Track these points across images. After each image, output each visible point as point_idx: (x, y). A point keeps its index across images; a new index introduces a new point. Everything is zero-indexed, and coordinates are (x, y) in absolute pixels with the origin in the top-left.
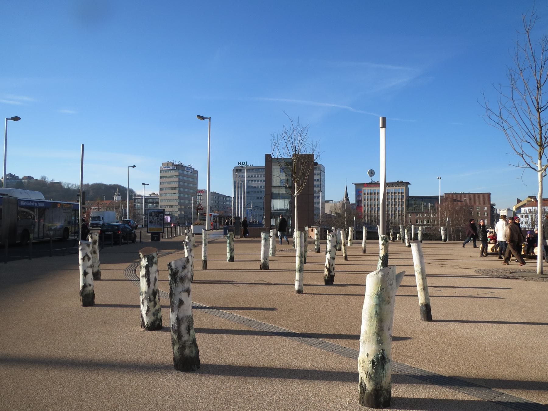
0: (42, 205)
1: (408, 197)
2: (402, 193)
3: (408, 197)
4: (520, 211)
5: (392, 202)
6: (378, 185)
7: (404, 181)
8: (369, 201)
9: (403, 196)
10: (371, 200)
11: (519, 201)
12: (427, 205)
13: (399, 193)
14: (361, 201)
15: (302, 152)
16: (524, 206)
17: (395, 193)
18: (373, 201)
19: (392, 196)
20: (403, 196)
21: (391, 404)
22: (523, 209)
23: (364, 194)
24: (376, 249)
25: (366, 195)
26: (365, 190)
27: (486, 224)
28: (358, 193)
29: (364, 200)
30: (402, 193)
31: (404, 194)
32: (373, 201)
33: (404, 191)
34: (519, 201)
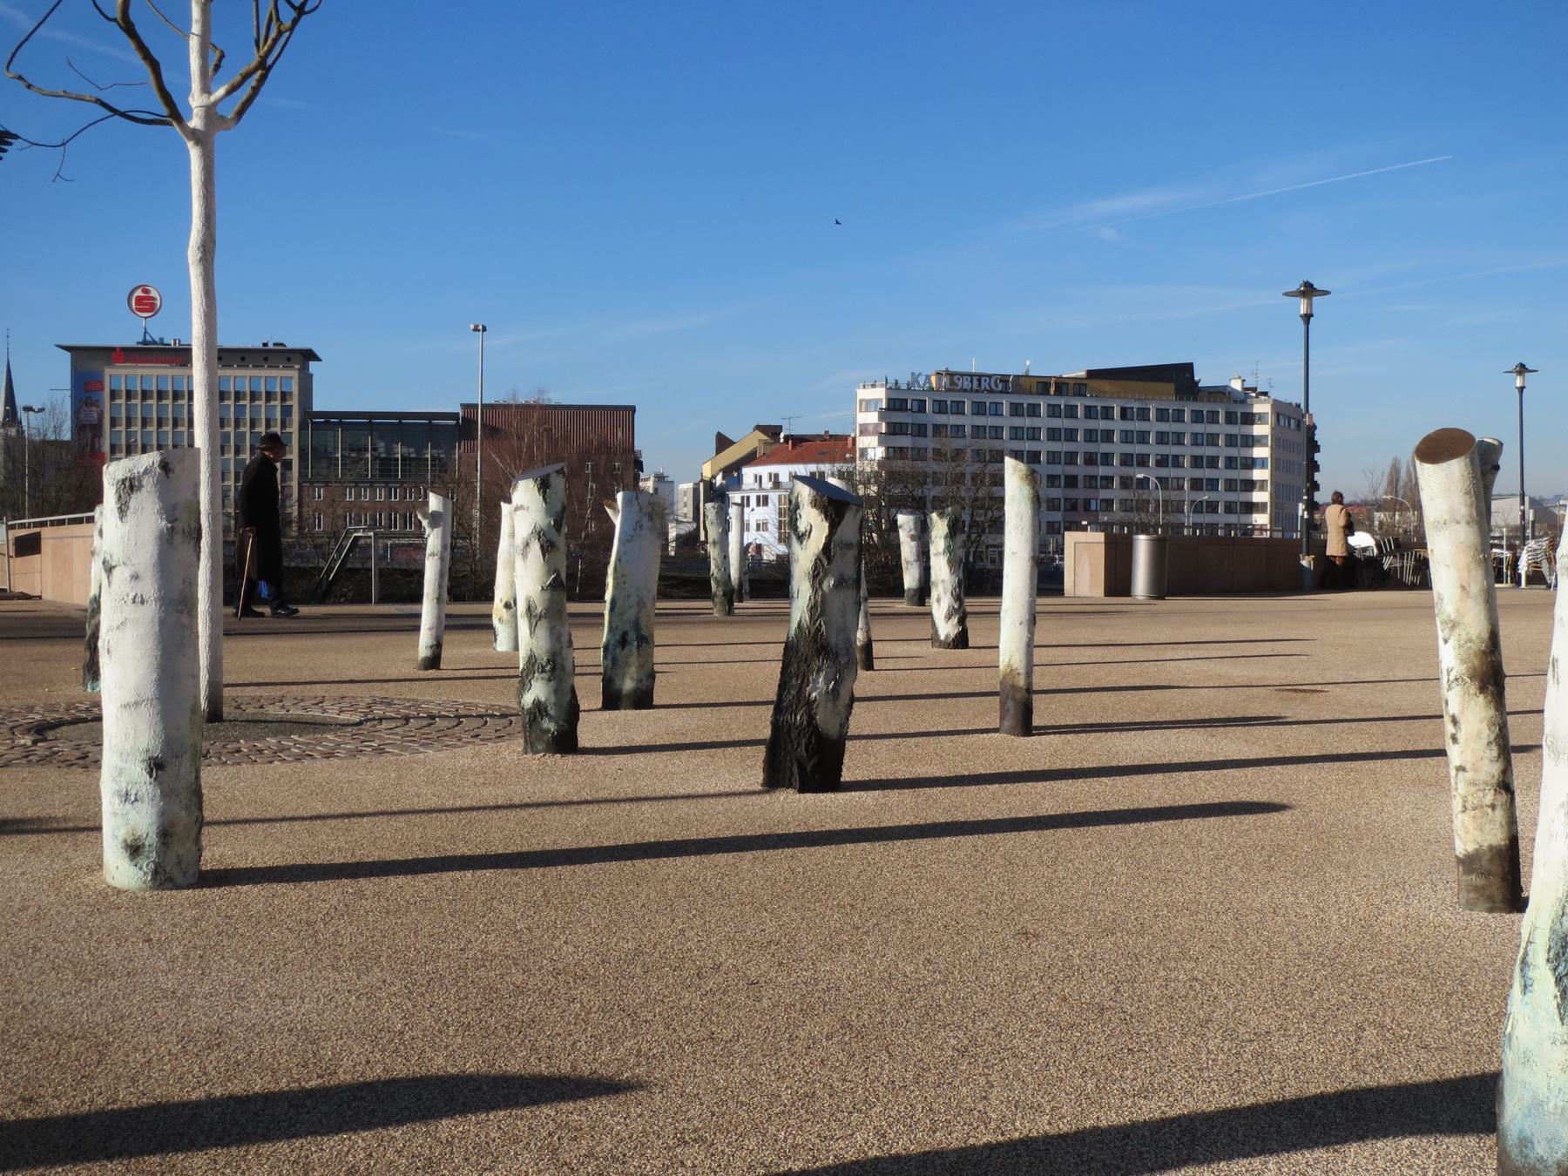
0: (702, 538)
1: (308, 415)
2: (285, 396)
3: (308, 415)
4: (739, 480)
5: (240, 437)
6: (181, 356)
7: (290, 345)
8: (137, 428)
9: (287, 411)
10: (145, 422)
11: (723, 443)
12: (389, 450)
13: (269, 396)
14: (97, 429)
15: (1471, 1141)
16: (750, 459)
17: (254, 396)
18: (168, 428)
19: (240, 410)
20: (287, 411)
21: (401, 561)
22: (748, 473)
23: (114, 395)
24: (70, 692)
25: (122, 401)
26: (116, 376)
27: (710, 540)
28: (85, 387)
29: (114, 422)
30: (285, 396)
31: (294, 402)
32: (153, 428)
33: (295, 389)
34: (723, 443)
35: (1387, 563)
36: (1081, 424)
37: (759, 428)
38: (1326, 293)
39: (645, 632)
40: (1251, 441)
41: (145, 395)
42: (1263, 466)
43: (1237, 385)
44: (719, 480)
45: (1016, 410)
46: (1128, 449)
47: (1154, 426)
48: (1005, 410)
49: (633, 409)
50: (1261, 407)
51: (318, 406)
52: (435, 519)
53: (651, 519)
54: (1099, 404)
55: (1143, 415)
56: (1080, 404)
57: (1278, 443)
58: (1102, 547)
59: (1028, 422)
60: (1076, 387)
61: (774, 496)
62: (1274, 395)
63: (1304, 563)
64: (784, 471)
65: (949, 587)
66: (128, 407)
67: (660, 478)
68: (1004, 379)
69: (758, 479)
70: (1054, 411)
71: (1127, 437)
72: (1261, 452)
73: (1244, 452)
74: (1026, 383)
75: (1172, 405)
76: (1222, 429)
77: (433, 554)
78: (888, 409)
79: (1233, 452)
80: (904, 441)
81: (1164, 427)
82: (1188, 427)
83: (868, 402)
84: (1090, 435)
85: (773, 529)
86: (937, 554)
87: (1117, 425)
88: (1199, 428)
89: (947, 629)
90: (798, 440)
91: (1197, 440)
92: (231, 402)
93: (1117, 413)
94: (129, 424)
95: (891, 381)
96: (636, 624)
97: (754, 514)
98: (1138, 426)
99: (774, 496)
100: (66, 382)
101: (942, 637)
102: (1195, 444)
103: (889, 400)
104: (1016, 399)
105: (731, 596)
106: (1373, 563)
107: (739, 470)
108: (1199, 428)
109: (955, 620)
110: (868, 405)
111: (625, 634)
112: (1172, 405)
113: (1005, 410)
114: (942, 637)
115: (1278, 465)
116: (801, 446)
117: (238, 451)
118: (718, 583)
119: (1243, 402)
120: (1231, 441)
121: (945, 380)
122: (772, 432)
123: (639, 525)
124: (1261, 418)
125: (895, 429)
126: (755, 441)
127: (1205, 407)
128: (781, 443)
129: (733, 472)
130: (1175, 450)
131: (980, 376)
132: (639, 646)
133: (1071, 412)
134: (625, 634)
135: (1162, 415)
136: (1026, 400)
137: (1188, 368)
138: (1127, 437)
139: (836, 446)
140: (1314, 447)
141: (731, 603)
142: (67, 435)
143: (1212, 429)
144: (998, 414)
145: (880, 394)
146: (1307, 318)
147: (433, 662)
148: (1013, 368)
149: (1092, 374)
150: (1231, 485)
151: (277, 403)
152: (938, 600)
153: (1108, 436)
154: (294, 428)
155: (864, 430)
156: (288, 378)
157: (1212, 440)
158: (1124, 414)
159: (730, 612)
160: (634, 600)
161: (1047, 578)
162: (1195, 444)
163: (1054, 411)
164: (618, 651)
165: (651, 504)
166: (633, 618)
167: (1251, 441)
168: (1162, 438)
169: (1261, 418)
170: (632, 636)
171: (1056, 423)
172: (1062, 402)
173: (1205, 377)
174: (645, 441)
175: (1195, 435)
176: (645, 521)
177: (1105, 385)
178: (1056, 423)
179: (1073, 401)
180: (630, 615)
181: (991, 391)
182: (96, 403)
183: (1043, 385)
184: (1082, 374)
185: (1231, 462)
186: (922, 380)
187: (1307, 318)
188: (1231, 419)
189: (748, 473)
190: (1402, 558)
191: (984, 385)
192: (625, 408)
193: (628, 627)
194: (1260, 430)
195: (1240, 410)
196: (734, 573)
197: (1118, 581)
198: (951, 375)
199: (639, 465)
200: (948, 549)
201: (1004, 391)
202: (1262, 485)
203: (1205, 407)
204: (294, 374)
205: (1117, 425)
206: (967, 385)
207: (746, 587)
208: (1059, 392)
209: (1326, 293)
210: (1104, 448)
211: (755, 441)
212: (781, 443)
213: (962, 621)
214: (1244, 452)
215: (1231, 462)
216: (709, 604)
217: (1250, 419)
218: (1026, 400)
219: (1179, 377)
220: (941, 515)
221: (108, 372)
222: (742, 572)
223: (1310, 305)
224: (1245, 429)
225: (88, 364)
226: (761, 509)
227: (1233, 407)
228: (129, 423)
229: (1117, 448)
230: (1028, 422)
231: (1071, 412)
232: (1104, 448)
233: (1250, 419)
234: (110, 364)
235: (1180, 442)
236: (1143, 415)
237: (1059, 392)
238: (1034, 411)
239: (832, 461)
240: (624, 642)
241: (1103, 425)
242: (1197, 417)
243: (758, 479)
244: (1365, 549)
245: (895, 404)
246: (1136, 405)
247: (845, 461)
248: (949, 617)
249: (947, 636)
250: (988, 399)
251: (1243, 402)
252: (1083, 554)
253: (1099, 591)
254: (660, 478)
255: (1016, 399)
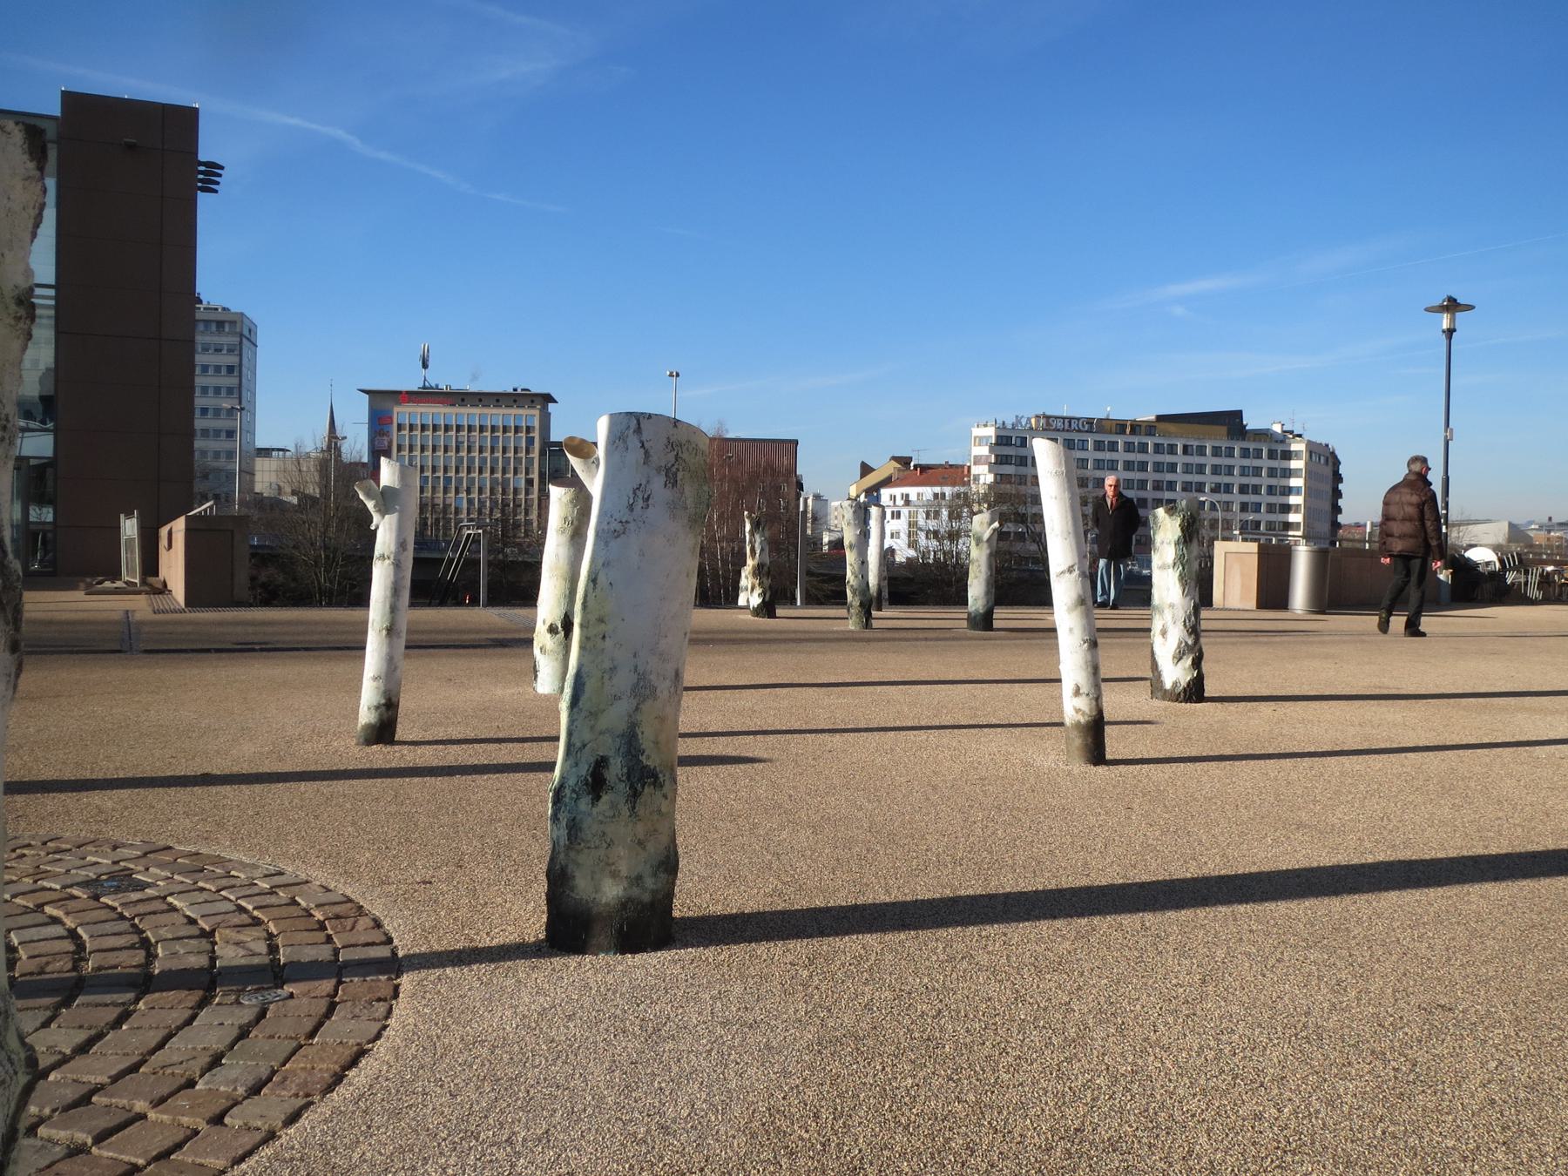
3: (546, 444)
4: (878, 498)
7: (534, 390)
9: (530, 441)
10: (423, 449)
11: (866, 470)
18: (440, 453)
19: (494, 439)
20: (530, 441)
22: (885, 494)
23: (400, 427)
28: (379, 423)
31: (536, 435)
32: (429, 453)
33: (536, 424)
34: (866, 470)
35: (1510, 577)
36: (1150, 458)
37: (894, 458)
38: (1470, 308)
39: (651, 760)
40: (1288, 473)
41: (424, 428)
42: (1298, 493)
43: (1277, 428)
44: (862, 498)
45: (1099, 446)
46: (1189, 478)
47: (1209, 460)
48: (1090, 446)
49: (796, 442)
50: (1298, 446)
51: (553, 438)
52: (388, 500)
53: (672, 480)
54: (1166, 442)
55: (1201, 451)
56: (1150, 442)
57: (1310, 475)
58: (1256, 557)
59: (1107, 456)
60: (1149, 428)
61: (905, 512)
62: (1306, 437)
63: (1441, 577)
64: (913, 492)
65: (1181, 615)
66: (411, 437)
67: (817, 497)
68: (1090, 421)
69: (893, 498)
70: (1129, 447)
71: (1188, 468)
72: (1296, 482)
73: (1283, 482)
74: (1107, 425)
75: (1224, 444)
76: (1265, 463)
77: (383, 557)
78: (997, 444)
79: (1273, 482)
80: (1009, 469)
81: (1217, 461)
82: (1237, 461)
83: (981, 438)
84: (1158, 467)
85: (904, 536)
86: (1163, 567)
87: (1180, 459)
88: (1246, 462)
89: (1175, 674)
90: (924, 468)
91: (1244, 471)
92: (488, 434)
93: (1179, 450)
94: (411, 450)
95: (1000, 422)
96: (630, 741)
97: (892, 525)
98: (1196, 460)
99: (905, 512)
100: (365, 417)
101: (1168, 685)
102: (1242, 475)
103: (998, 437)
104: (1099, 437)
105: (868, 606)
106: (1497, 577)
107: (878, 490)
108: (1246, 462)
109: (1188, 661)
110: (980, 440)
111: (601, 763)
112: (1224, 444)
113: (1090, 446)
114: (1168, 685)
115: (1310, 493)
116: (925, 473)
117: (493, 471)
118: (854, 592)
119: (1282, 442)
120: (1272, 472)
121: (1042, 421)
122: (905, 461)
123: (641, 496)
124: (1297, 455)
125: (1001, 460)
126: (890, 468)
127: (1252, 446)
128: (910, 470)
129: (873, 492)
130: (1227, 480)
131: (1071, 419)
132: (635, 795)
133: (1143, 448)
134: (601, 763)
135: (1216, 452)
136: (1107, 438)
137: (1238, 415)
138: (1188, 468)
139: (954, 473)
140: (1338, 478)
141: (868, 616)
142: (365, 460)
143: (1257, 463)
144: (1084, 449)
145: (990, 432)
146: (1450, 332)
147: (383, 731)
148: (1096, 413)
149: (1160, 418)
150: (1271, 508)
151: (523, 435)
152: (1164, 633)
153: (1172, 468)
154: (535, 454)
155: (978, 460)
156: (531, 416)
157: (1257, 471)
158: (1186, 449)
159: (867, 625)
160: (624, 680)
161: (1200, 585)
162: (1242, 475)
163: (1129, 447)
164: (584, 804)
165: (671, 445)
166: (622, 726)
167: (1288, 473)
168: (1216, 470)
169: (1297, 455)
170: (616, 769)
171: (1131, 457)
172: (1136, 440)
173: (1251, 422)
174: (805, 467)
175: (1243, 468)
176: (658, 484)
177: (1171, 427)
178: (1131, 457)
179: (1145, 439)
180: (616, 717)
181: (1079, 431)
182: (388, 434)
183: (1121, 427)
184: (1153, 418)
185: (1271, 490)
186: (1024, 422)
187: (1450, 332)
188: (1272, 455)
189: (885, 494)
190: (1526, 572)
191: (1074, 425)
192: (791, 441)
193: (608, 746)
194: (1296, 464)
195: (1280, 448)
196: (873, 580)
197: (1273, 592)
198: (1047, 417)
199: (800, 486)
200: (1181, 560)
201: (1090, 431)
202: (1297, 508)
203: (1252, 446)
204: (536, 412)
205: (1180, 459)
206: (1060, 425)
207: (885, 594)
208: (1133, 432)
209: (1470, 308)
210: (1169, 477)
211: (890, 468)
212: (910, 470)
213: (1197, 663)
214: (1283, 482)
215: (1271, 490)
216: (842, 612)
217: (1288, 455)
218: (1107, 438)
219: (1231, 422)
220: (1171, 511)
221: (396, 409)
222: (881, 578)
223: (1453, 320)
224: (1284, 464)
225: (382, 403)
226: (895, 521)
227: (1276, 446)
228: (411, 450)
229: (1180, 477)
230: (1107, 456)
231: (1143, 448)
232: (1169, 477)
233: (1288, 455)
234: (399, 403)
235: (1230, 473)
236: (1201, 451)
237: (1133, 432)
238: (1113, 447)
239: (953, 485)
240: (596, 783)
241: (1168, 458)
242: (1245, 453)
243: (893, 498)
244: (1488, 564)
245: (1002, 440)
246: (1195, 443)
247: (964, 484)
248: (1179, 657)
249: (1175, 684)
250: (1076, 437)
251: (1282, 442)
252: (1235, 564)
253: (1252, 603)
254: (817, 497)
255: (1099, 437)
